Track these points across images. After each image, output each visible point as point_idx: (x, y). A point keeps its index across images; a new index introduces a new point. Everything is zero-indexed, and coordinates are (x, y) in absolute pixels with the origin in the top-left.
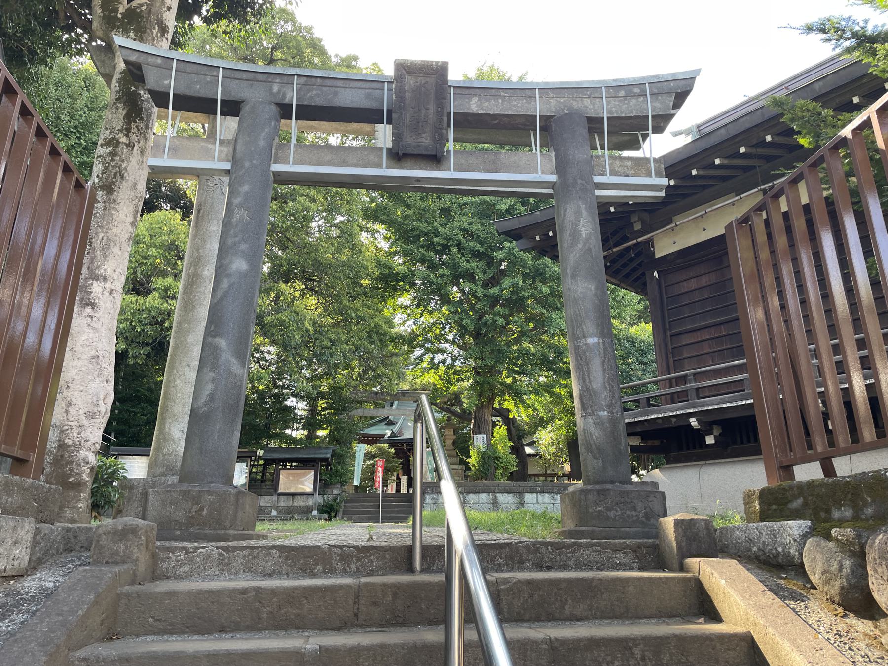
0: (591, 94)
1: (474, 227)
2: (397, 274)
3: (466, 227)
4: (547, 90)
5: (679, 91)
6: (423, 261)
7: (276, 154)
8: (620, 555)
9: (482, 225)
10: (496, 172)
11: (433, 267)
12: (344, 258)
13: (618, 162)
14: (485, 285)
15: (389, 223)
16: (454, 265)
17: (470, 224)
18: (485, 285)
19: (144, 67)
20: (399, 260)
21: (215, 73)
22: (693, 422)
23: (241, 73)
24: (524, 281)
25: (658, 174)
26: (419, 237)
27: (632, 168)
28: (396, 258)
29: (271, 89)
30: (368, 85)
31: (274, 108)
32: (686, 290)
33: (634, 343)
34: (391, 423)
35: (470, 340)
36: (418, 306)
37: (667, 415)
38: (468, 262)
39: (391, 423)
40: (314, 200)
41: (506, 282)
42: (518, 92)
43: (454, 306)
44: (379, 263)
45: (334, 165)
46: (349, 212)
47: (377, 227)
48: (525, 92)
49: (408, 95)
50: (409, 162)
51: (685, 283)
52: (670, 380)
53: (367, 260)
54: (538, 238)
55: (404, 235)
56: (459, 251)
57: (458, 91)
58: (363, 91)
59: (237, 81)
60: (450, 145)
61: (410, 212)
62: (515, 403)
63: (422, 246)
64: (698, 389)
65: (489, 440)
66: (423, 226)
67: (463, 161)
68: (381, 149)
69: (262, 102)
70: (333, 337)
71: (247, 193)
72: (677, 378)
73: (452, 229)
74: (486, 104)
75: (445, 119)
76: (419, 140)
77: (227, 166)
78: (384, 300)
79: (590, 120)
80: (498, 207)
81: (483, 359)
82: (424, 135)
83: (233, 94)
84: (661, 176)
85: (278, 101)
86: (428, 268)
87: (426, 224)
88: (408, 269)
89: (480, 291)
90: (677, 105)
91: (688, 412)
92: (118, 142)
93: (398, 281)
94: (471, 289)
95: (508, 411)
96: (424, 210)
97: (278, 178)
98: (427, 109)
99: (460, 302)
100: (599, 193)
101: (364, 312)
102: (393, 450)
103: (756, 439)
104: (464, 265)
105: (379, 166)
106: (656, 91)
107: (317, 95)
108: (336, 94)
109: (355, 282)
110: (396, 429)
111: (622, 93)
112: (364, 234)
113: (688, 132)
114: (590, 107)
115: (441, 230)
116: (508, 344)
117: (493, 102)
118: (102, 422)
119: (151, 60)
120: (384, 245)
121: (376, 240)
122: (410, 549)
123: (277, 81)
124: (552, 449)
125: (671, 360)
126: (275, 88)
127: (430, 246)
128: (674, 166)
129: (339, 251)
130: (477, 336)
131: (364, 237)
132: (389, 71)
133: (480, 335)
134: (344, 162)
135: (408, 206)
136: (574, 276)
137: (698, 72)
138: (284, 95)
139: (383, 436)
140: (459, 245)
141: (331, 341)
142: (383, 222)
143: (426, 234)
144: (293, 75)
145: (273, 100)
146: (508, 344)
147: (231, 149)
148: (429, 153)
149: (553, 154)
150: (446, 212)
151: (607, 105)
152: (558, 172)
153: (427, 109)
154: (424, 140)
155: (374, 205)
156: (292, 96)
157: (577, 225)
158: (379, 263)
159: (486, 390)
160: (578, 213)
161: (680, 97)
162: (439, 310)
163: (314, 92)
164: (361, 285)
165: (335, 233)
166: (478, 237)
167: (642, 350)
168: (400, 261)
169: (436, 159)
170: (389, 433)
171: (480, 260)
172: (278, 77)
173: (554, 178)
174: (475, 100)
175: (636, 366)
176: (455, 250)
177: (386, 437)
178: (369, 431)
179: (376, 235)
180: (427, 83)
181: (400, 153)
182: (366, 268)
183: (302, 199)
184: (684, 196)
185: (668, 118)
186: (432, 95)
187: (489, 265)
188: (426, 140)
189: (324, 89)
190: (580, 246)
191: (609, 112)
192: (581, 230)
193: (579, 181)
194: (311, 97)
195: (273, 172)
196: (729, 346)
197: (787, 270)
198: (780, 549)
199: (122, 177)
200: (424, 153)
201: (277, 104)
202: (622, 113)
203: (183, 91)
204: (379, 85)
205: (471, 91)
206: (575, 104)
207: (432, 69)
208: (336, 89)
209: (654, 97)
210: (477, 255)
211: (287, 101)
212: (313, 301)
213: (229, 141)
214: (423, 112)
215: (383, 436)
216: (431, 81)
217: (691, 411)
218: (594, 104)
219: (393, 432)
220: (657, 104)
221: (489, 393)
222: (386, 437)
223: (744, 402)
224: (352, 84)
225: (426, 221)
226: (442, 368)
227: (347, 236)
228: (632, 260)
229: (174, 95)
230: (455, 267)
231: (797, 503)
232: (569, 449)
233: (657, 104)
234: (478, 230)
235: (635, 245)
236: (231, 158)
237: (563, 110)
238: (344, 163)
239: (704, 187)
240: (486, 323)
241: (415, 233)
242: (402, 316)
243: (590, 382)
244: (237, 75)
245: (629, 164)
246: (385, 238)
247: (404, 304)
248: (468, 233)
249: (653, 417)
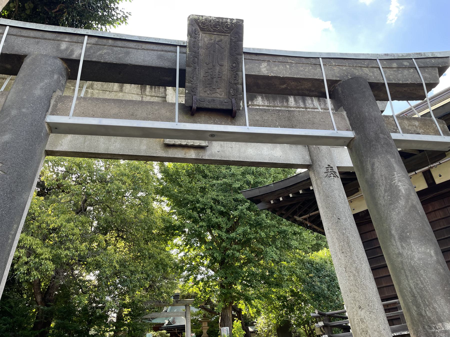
0: (368, 65)
1: (220, 198)
2: (175, 226)
3: (215, 197)
4: (330, 60)
6: (190, 218)
7: (55, 106)
9: (224, 196)
10: (293, 127)
11: (195, 221)
12: (142, 217)
13: (406, 122)
14: (228, 231)
15: (170, 196)
16: (209, 220)
17: (218, 196)
18: (228, 231)
20: (175, 217)
23: (29, 31)
24: (250, 229)
26: (188, 203)
27: (421, 128)
28: (174, 216)
29: (59, 46)
30: (160, 47)
31: (59, 63)
33: (312, 264)
35: (217, 265)
36: (186, 245)
38: (217, 218)
40: (124, 183)
41: (240, 230)
42: (304, 59)
43: (208, 245)
44: (164, 220)
45: (121, 118)
46: (146, 190)
47: (163, 198)
49: (202, 52)
50: (203, 117)
53: (157, 218)
54: (272, 202)
55: (179, 203)
56: (211, 211)
58: (155, 53)
59: (23, 39)
61: (182, 189)
62: (246, 305)
63: (189, 209)
65: (230, 330)
66: (190, 197)
67: (258, 118)
68: (174, 104)
69: (46, 55)
70: (133, 269)
71: (7, 143)
73: (207, 199)
74: (276, 69)
76: (214, 95)
78: (166, 241)
80: (233, 186)
81: (226, 278)
82: (218, 91)
83: (16, 48)
85: (65, 56)
86: (193, 222)
87: (192, 196)
88: (181, 223)
89: (224, 236)
93: (175, 230)
94: (219, 235)
95: (241, 310)
96: (191, 188)
98: (221, 65)
99: (212, 242)
101: (153, 250)
102: (169, 334)
104: (215, 220)
105: (172, 120)
106: (423, 65)
107: (109, 54)
108: (128, 53)
109: (149, 231)
111: (395, 65)
112: (155, 203)
114: (372, 76)
115: (201, 199)
116: (241, 267)
117: (281, 67)
120: (167, 209)
121: (162, 206)
123: (66, 40)
124: (266, 330)
126: (64, 46)
127: (194, 209)
129: (139, 212)
130: (222, 263)
131: (155, 204)
132: (180, 34)
133: (224, 263)
134: (132, 115)
135: (181, 186)
136: (403, 239)
138: (72, 52)
139: (163, 324)
140: (211, 208)
141: (131, 271)
142: (166, 196)
143: (192, 202)
145: (60, 56)
146: (241, 267)
148: (224, 107)
149: (345, 113)
150: (203, 190)
151: (385, 74)
152: (354, 128)
153: (221, 65)
154: (219, 96)
155: (161, 186)
157: (392, 180)
158: (164, 220)
159: (228, 297)
160: (389, 167)
162: (200, 247)
163: (105, 51)
164: (153, 233)
165: (137, 202)
166: (222, 203)
167: (317, 269)
168: (176, 218)
170: (167, 322)
171: (224, 217)
172: (67, 36)
173: (350, 134)
174: (264, 65)
175: (316, 279)
176: (209, 211)
177: (165, 325)
179: (162, 203)
180: (221, 41)
181: (194, 106)
182: (155, 223)
183: (117, 182)
186: (227, 53)
187: (229, 219)
188: (219, 97)
189: (115, 49)
190: (402, 202)
191: (388, 79)
193: (381, 136)
194: (101, 55)
195: (48, 124)
200: (219, 107)
201: (62, 59)
202: (399, 80)
204: (172, 48)
206: (357, 72)
207: (227, 26)
208: (128, 50)
209: (422, 69)
210: (222, 214)
211: (74, 57)
212: (121, 244)
214: (218, 68)
215: (163, 324)
216: (226, 39)
218: (373, 73)
219: (169, 322)
221: (230, 300)
222: (165, 325)
225: (192, 194)
226: (201, 284)
227: (145, 202)
230: (209, 220)
232: (277, 332)
234: (222, 199)
237: (347, 76)
240: (228, 255)
241: (185, 201)
242: (176, 249)
246: (167, 205)
247: (178, 243)
248: (216, 201)
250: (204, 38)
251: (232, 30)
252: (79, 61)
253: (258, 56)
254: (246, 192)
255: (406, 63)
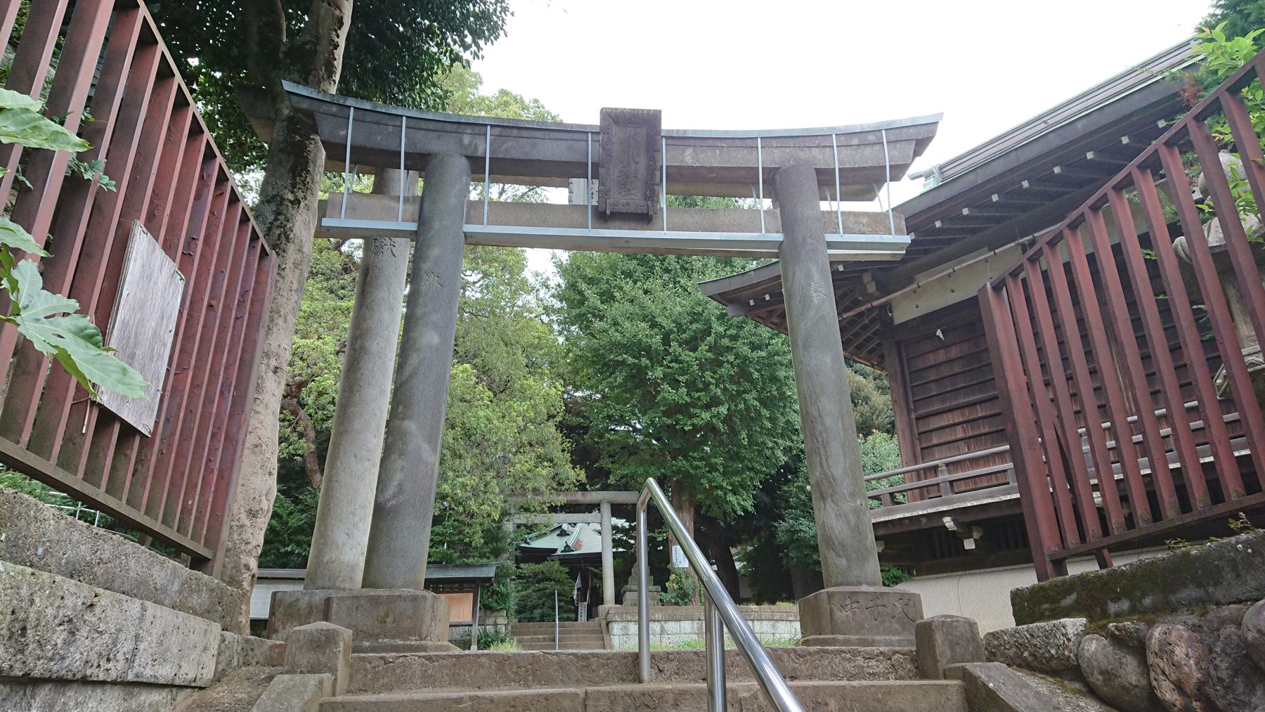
4: (772, 140)
5: (919, 137)
7: (468, 213)
8: (873, 663)
19: (317, 117)
21: (398, 123)
22: (948, 522)
25: (898, 232)
27: (868, 225)
29: (461, 140)
31: (464, 160)
32: (932, 363)
34: (563, 534)
37: (915, 514)
39: (563, 534)
48: (745, 142)
51: (931, 356)
52: (917, 471)
57: (671, 142)
58: (564, 143)
60: (663, 200)
64: (951, 482)
72: (925, 469)
75: (658, 173)
77: (413, 227)
79: (819, 172)
84: (902, 234)
90: (917, 153)
91: (943, 506)
92: (283, 199)
97: (469, 240)
100: (830, 252)
103: (1026, 543)
108: (534, 145)
110: (571, 541)
113: (928, 175)
114: (820, 158)
117: (710, 153)
118: (264, 522)
119: (325, 107)
122: (636, 657)
125: (918, 448)
128: (916, 217)
132: (594, 120)
137: (941, 115)
138: (476, 146)
139: (555, 550)
144: (486, 125)
147: (417, 207)
152: (784, 231)
156: (486, 148)
161: (920, 145)
163: (510, 144)
169: (645, 218)
173: (779, 237)
174: (689, 151)
178: (537, 544)
184: (926, 252)
185: (904, 167)
188: (635, 201)
192: (816, 299)
196: (987, 430)
197: (957, 417)
198: (1053, 652)
199: (287, 238)
203: (362, 142)
204: (583, 136)
205: (687, 142)
206: (803, 155)
211: (479, 154)
213: (415, 198)
214: (633, 165)
216: (643, 132)
217: (945, 509)
220: (896, 153)
222: (559, 553)
223: (1008, 497)
224: (553, 135)
228: (865, 328)
229: (352, 147)
231: (1069, 600)
233: (896, 153)
235: (869, 310)
236: (417, 217)
238: (545, 223)
239: (949, 242)
243: (829, 467)
244: (423, 125)
245: (865, 220)
249: (899, 516)
250: (617, 133)
251: (646, 122)
252: (484, 158)
253: (681, 140)
254: (1153, 87)
255: (871, 138)
